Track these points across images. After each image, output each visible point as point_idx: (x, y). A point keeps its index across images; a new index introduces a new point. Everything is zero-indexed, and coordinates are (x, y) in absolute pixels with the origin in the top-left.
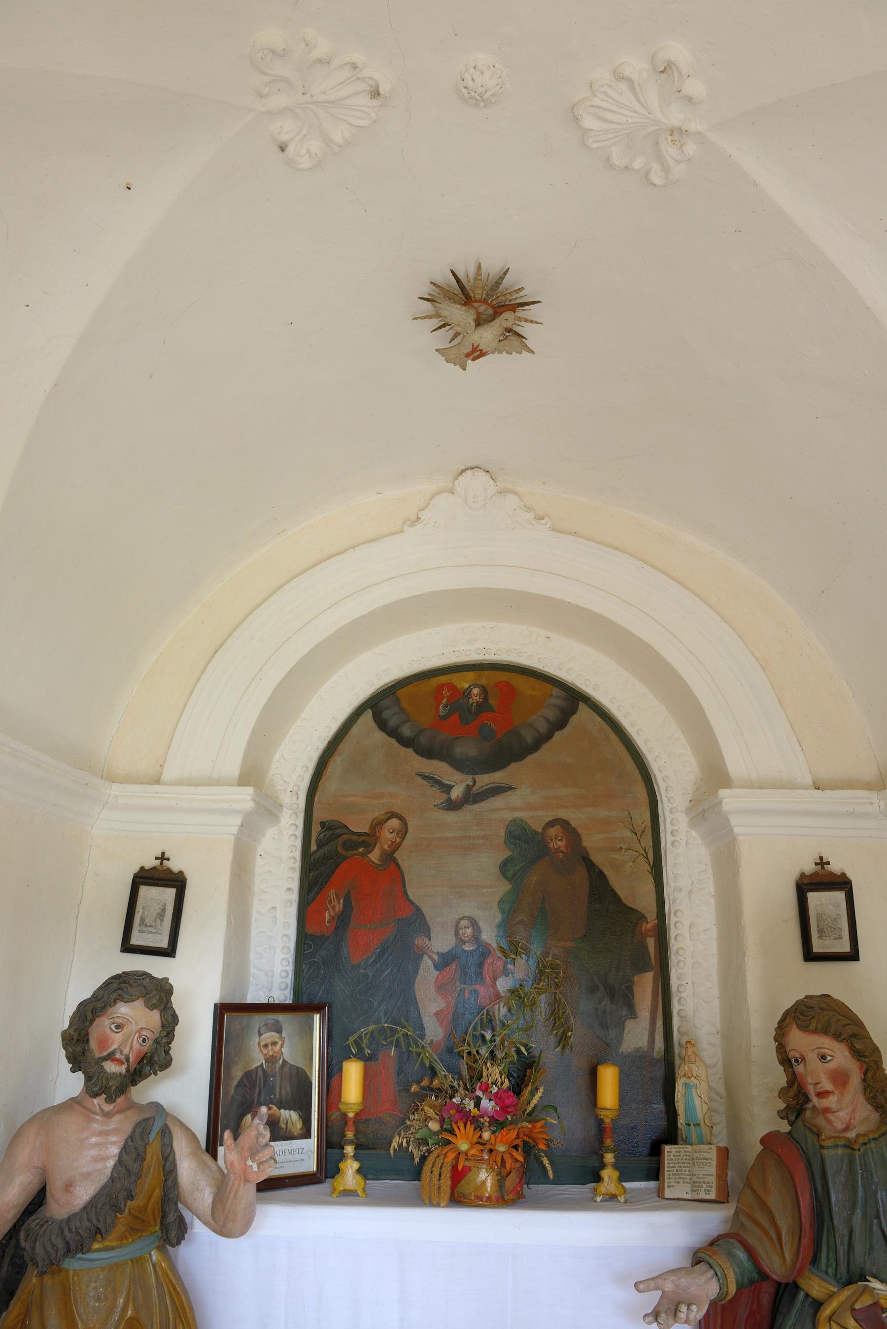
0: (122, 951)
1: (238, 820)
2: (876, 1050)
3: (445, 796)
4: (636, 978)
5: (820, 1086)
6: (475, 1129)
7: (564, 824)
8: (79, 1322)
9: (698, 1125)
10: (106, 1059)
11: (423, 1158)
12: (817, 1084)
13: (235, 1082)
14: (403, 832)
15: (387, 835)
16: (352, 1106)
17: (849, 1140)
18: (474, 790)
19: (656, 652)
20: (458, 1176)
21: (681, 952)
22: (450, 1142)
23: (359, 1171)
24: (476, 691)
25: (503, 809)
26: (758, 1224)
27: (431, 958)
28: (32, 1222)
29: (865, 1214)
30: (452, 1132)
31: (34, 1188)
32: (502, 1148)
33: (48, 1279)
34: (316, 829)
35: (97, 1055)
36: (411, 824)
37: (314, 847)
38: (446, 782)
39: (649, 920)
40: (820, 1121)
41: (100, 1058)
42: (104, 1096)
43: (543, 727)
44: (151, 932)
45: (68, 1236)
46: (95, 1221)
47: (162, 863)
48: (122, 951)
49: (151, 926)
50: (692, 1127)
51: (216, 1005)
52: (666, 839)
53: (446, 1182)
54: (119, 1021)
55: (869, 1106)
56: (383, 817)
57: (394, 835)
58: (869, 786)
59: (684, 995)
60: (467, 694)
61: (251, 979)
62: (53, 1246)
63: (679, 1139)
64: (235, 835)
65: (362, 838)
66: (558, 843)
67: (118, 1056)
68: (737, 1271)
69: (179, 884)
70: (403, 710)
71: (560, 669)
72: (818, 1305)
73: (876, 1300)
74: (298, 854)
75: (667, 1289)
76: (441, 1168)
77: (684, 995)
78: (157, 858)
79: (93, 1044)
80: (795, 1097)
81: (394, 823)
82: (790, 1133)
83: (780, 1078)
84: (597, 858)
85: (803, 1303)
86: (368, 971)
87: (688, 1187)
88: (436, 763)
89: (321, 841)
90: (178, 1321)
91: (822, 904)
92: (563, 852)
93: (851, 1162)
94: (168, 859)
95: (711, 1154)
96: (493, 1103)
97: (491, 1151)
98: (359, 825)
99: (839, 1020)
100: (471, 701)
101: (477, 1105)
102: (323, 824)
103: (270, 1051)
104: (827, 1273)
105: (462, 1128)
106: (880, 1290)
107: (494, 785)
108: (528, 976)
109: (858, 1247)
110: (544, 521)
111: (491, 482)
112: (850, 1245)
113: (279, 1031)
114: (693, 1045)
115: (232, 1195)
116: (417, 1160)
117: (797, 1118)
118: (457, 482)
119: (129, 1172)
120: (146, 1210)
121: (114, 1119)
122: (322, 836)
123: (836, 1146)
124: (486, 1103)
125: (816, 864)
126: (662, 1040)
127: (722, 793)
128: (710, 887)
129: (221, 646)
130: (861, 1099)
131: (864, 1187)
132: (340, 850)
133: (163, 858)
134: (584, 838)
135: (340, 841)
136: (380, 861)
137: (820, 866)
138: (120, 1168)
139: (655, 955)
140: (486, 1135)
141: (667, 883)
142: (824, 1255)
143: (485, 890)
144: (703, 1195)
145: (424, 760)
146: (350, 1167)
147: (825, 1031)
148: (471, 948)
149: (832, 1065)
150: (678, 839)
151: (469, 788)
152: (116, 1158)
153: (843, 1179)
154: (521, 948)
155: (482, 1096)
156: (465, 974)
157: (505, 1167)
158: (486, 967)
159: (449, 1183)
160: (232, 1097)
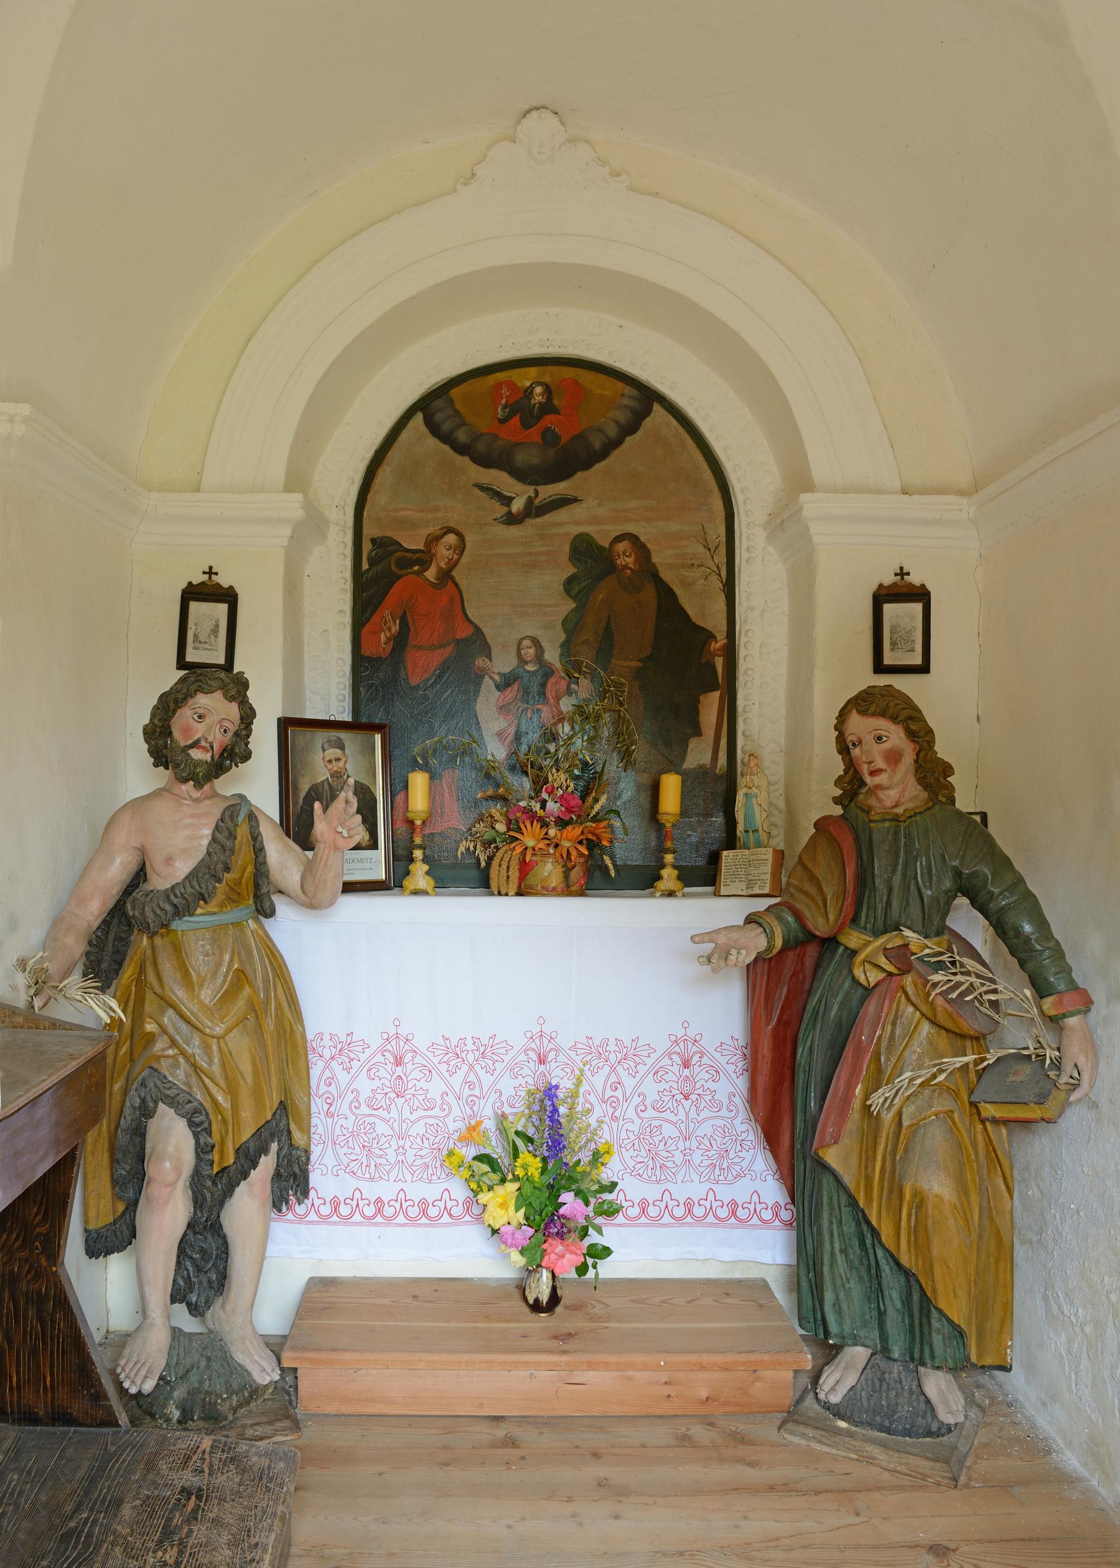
0: (177, 669)
1: (287, 531)
2: (930, 732)
3: (505, 509)
4: (702, 698)
5: (873, 765)
6: (541, 827)
7: (633, 539)
8: (192, 972)
9: (756, 831)
10: (192, 746)
11: (490, 859)
12: (870, 763)
13: (302, 795)
14: (461, 547)
15: (443, 552)
16: (284, 1122)
17: (896, 814)
18: (537, 501)
19: (743, 340)
20: (525, 868)
21: (749, 672)
22: (517, 839)
23: (427, 873)
24: (538, 390)
25: (568, 523)
26: (806, 894)
27: (491, 678)
28: (137, 894)
29: (904, 876)
30: (519, 830)
31: (133, 867)
32: (566, 844)
33: (158, 940)
34: (367, 547)
35: (182, 744)
36: (468, 539)
37: (365, 566)
38: (506, 493)
39: (718, 639)
40: (872, 801)
41: (185, 746)
42: (192, 783)
43: (612, 431)
44: (206, 649)
45: (175, 901)
46: (197, 888)
47: (210, 578)
48: (177, 669)
49: (205, 642)
50: (751, 834)
51: (279, 719)
52: (740, 556)
53: (514, 874)
54: (201, 711)
55: (919, 787)
56: (439, 533)
57: (451, 551)
58: (961, 493)
59: (749, 715)
60: (528, 393)
61: (308, 702)
62: (162, 909)
63: (738, 845)
64: (284, 547)
65: (417, 555)
66: (626, 559)
67: (203, 743)
68: (784, 929)
69: (231, 599)
70: (457, 412)
71: (633, 364)
72: (854, 953)
73: (907, 942)
74: (348, 575)
75: (719, 942)
76: (509, 861)
77: (749, 715)
78: (204, 573)
79: (176, 734)
80: (850, 782)
81: (451, 538)
82: (842, 815)
83: (839, 768)
84: (666, 575)
85: (842, 956)
86: (428, 692)
87: (743, 885)
88: (494, 472)
89: (372, 559)
90: (277, 978)
91: (897, 616)
92: (630, 569)
93: (896, 833)
94: (216, 574)
95: (768, 855)
96: (558, 805)
97: (557, 846)
98: (413, 542)
99: (897, 704)
100: (533, 401)
101: (543, 807)
102: (373, 541)
103: (335, 766)
104: (865, 928)
105: (529, 826)
106: (912, 938)
107: (558, 497)
108: (592, 695)
109: (895, 904)
110: (621, 178)
111: (561, 128)
112: (889, 903)
113: (342, 748)
114: (756, 757)
115: (323, 862)
116: (483, 864)
117: (850, 802)
118: (519, 127)
119: (223, 848)
120: (240, 883)
121: (202, 804)
122: (373, 554)
123: (884, 820)
124: (551, 805)
125: (896, 575)
126: (725, 757)
127: (803, 497)
128: (784, 605)
129: (253, 335)
130: (912, 780)
131: (906, 852)
132: (393, 568)
133: (210, 572)
134: (653, 554)
135: (394, 558)
136: (437, 579)
137: (899, 577)
138: (214, 845)
139: (723, 675)
140: (552, 832)
141: (739, 603)
142: (864, 914)
143: (548, 609)
144: (757, 891)
145: (481, 469)
146: (419, 869)
147: (883, 714)
148: (534, 669)
149: (886, 746)
150: (753, 555)
151: (530, 501)
152: (210, 838)
153: (887, 848)
154: (586, 667)
155: (547, 799)
156: (528, 694)
157: (570, 859)
158: (549, 687)
159: (517, 874)
160: (301, 807)
